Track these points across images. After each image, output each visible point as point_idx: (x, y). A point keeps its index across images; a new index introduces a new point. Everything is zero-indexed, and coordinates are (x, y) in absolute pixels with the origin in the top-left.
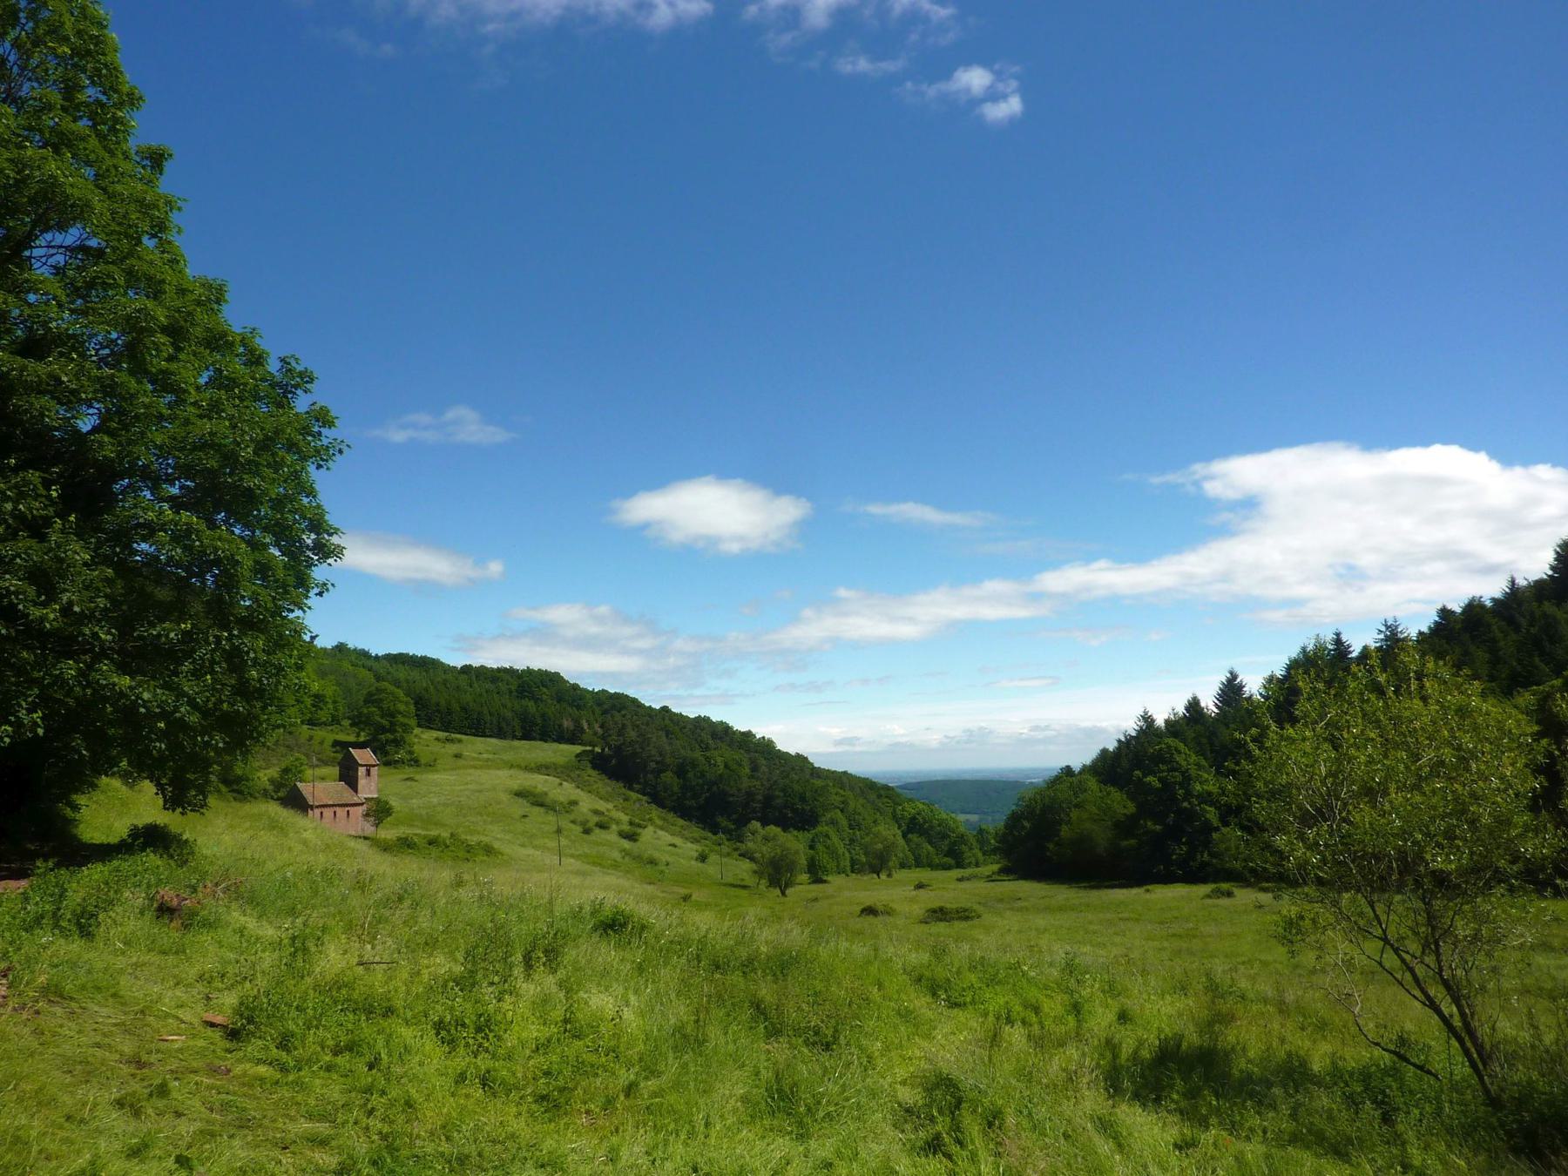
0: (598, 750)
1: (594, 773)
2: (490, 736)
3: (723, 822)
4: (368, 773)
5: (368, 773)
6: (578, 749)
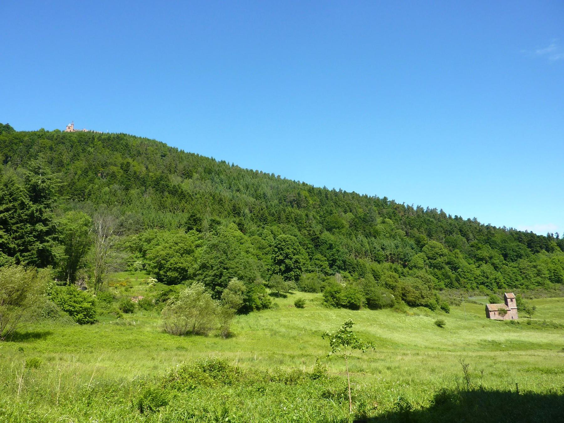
4: (512, 301)
5: (512, 301)
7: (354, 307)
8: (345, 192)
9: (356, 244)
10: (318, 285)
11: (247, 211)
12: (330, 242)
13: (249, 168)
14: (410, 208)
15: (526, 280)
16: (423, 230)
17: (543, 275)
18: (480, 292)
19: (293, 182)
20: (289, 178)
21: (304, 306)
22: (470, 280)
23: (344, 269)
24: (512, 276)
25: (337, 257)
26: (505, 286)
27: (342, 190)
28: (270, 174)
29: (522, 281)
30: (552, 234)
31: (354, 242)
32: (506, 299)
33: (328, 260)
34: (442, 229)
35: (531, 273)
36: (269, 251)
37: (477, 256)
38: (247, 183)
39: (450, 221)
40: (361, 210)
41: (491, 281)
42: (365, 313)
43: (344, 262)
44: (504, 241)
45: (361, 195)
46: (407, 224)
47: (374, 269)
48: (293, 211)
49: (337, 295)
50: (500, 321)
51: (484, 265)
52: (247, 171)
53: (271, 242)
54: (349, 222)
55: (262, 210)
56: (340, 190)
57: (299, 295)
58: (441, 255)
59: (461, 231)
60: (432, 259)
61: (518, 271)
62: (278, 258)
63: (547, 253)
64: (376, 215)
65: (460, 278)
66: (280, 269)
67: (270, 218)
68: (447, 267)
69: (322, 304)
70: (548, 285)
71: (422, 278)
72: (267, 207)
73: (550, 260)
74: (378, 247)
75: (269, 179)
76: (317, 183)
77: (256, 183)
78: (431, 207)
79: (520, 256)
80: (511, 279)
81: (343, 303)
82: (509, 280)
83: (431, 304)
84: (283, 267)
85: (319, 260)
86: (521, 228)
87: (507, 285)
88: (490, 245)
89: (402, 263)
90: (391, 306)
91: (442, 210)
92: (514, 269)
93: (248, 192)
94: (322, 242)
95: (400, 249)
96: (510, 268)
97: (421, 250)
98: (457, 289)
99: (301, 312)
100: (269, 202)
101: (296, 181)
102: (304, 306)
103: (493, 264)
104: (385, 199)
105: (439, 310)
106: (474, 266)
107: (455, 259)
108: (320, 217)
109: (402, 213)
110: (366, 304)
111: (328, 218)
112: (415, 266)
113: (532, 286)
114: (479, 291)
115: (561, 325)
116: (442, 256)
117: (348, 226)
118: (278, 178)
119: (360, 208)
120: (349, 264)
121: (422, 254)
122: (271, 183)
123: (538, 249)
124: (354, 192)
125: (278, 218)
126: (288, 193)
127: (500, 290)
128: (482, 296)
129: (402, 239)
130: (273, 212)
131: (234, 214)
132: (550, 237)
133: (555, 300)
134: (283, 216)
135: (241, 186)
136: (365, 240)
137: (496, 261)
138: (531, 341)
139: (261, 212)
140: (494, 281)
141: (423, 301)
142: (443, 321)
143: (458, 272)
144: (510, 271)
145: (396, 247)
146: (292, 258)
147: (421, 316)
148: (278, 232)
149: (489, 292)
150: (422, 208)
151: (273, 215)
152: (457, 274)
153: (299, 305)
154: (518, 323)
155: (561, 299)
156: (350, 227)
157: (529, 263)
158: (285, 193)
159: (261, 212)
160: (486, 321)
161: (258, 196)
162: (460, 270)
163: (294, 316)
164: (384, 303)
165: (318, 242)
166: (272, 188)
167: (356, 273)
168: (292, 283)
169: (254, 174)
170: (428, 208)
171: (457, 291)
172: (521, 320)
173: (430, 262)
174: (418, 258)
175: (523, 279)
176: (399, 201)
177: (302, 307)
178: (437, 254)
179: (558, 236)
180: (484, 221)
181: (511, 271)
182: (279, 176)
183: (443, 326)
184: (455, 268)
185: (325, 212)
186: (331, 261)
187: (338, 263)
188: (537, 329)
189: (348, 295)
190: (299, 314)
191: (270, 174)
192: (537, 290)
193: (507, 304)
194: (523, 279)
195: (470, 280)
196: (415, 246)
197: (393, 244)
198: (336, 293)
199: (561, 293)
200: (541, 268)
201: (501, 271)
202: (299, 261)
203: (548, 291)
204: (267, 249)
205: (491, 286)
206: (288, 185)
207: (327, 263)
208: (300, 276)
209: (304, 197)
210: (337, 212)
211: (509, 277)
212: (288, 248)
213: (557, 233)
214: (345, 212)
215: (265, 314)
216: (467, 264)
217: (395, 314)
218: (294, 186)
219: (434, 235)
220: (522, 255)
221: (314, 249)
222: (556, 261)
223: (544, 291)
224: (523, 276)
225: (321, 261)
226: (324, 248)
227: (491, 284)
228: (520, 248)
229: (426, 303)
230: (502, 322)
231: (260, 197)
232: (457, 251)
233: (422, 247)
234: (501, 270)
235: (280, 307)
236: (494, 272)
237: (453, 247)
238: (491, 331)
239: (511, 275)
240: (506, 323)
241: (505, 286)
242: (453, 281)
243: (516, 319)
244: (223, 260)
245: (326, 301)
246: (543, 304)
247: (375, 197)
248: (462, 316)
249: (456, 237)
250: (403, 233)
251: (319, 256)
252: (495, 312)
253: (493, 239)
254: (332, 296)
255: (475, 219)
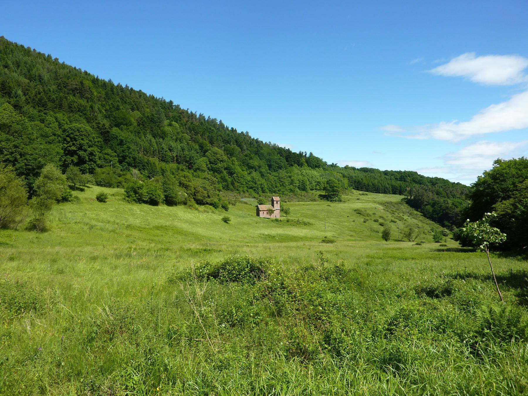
0: (409, 198)
1: (406, 205)
2: (381, 193)
3: (446, 223)
4: (277, 203)
5: (277, 203)
6: (403, 197)
7: (153, 202)
8: (132, 89)
9: (145, 143)
10: (115, 179)
11: (20, 92)
12: (121, 138)
13: (20, 43)
14: (192, 115)
16: (206, 137)
18: (249, 195)
19: (74, 69)
20: (68, 63)
21: (106, 200)
22: (242, 184)
23: (133, 167)
25: (127, 154)
26: (267, 191)
27: (128, 87)
28: (46, 55)
30: (303, 153)
31: (143, 140)
32: (273, 201)
33: (118, 156)
34: (221, 138)
35: (287, 182)
36: (54, 141)
37: (249, 164)
38: (17, 60)
39: (227, 132)
40: (148, 110)
42: (163, 208)
43: (134, 159)
44: (269, 154)
45: (148, 95)
46: (192, 129)
47: (163, 169)
48: (76, 100)
49: (140, 191)
51: (254, 173)
52: (17, 46)
53: (55, 131)
54: (137, 120)
55: (39, 94)
56: (127, 87)
57: (97, 190)
58: (222, 161)
59: (236, 142)
60: (213, 164)
62: (70, 149)
63: (298, 167)
64: (163, 116)
66: (72, 160)
67: (49, 104)
68: (225, 172)
69: (124, 199)
70: (297, 192)
71: (209, 180)
72: (44, 91)
73: (300, 173)
74: (166, 148)
75: (45, 60)
76: (103, 75)
77: (29, 62)
78: (212, 117)
79: (280, 168)
81: (144, 199)
83: (215, 203)
84: (75, 159)
85: (108, 154)
86: (281, 145)
87: (269, 190)
88: (259, 156)
89: (187, 165)
90: (185, 204)
91: (221, 121)
92: (275, 178)
93: (19, 70)
94: (112, 137)
95: (186, 152)
96: (272, 176)
97: (204, 155)
99: (105, 206)
100: (46, 86)
101: (77, 68)
102: (106, 200)
103: (261, 172)
104: (171, 102)
105: (220, 208)
106: (246, 173)
107: (232, 166)
108: (105, 111)
109: (186, 119)
110: (164, 200)
111: (116, 113)
112: (199, 169)
113: (286, 192)
115: (308, 223)
116: (222, 162)
117: (135, 124)
118: (55, 61)
119: (147, 108)
120: (139, 161)
121: (205, 158)
122: (47, 65)
123: (293, 163)
124: (140, 91)
125: (59, 105)
126: (70, 80)
127: (264, 194)
129: (188, 144)
130: (53, 98)
131: (3, 93)
132: (301, 154)
133: (302, 204)
134: (65, 104)
135: (9, 63)
136: (153, 140)
137: (263, 170)
138: (293, 234)
139: (39, 96)
140: (260, 186)
141: (209, 200)
143: (233, 177)
145: (182, 150)
146: (87, 150)
147: (210, 213)
148: (64, 120)
149: (256, 195)
150: (204, 117)
151: (53, 101)
153: (101, 199)
155: (306, 203)
156: (139, 125)
157: (286, 174)
158: (65, 80)
159: (39, 96)
160: (257, 219)
161: (32, 77)
162: (235, 175)
163: (99, 210)
164: (180, 201)
165: (108, 137)
166: (49, 71)
167: (146, 171)
168: (88, 176)
169: (27, 52)
170: (209, 117)
172: (282, 218)
173: (211, 167)
174: (202, 162)
176: (183, 107)
177: (104, 202)
178: (218, 159)
179: (306, 155)
180: (254, 135)
182: (56, 59)
183: (228, 222)
184: (231, 174)
185: (111, 106)
186: (121, 157)
187: (128, 160)
189: (150, 191)
190: (104, 208)
191: (46, 55)
193: (273, 205)
195: (242, 184)
196: (199, 151)
197: (179, 147)
198: (138, 189)
199: (305, 199)
202: (94, 154)
204: (51, 138)
206: (68, 71)
207: (117, 159)
208: (95, 169)
209: (88, 88)
210: (124, 109)
212: (82, 139)
213: (306, 152)
214: (133, 110)
215: (67, 207)
216: (241, 171)
217: (189, 210)
218: (74, 73)
219: (215, 143)
220: (282, 167)
221: (103, 143)
222: (304, 174)
224: (281, 184)
225: (111, 156)
226: (115, 143)
227: (258, 188)
228: (281, 161)
229: (211, 202)
231: (34, 78)
232: (234, 158)
233: (205, 152)
235: (82, 200)
236: (261, 179)
237: (230, 155)
239: (272, 182)
240: (272, 221)
241: (267, 191)
243: (278, 217)
244: (18, 143)
245: (127, 197)
247: (162, 99)
249: (233, 146)
250: (188, 137)
251: (109, 151)
253: (262, 151)
254: (136, 192)
255: (247, 133)
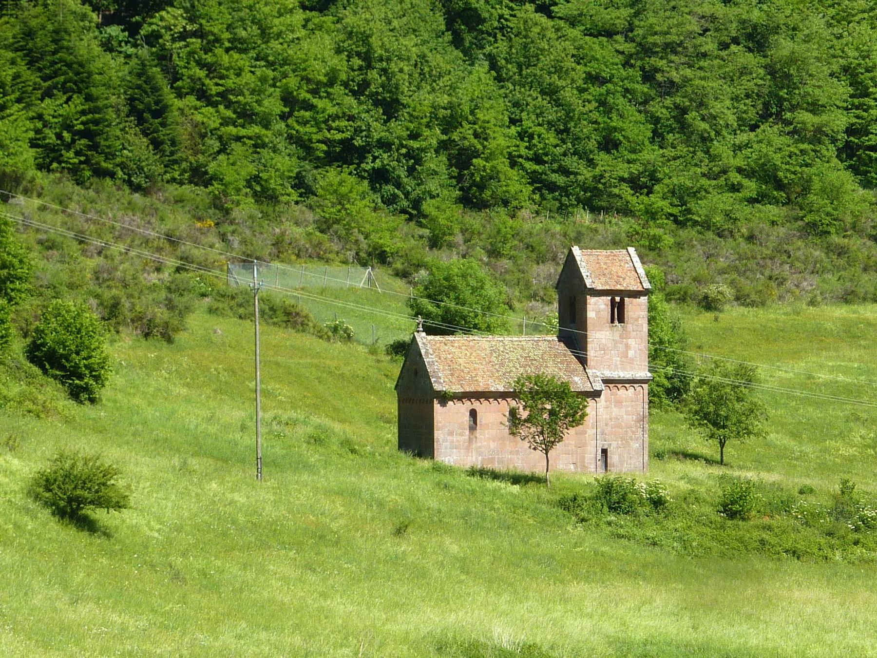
4: (618, 313)
5: (618, 313)
15: (682, 149)
17: (806, 117)
18: (324, 226)
22: (246, 116)
24: (579, 108)
29: (651, 154)
41: (414, 136)
50: (516, 479)
61: (626, 64)
65: (170, 98)
80: (563, 132)
82: (551, 138)
87: (534, 179)
92: (602, 49)
98: (136, 188)
114: (310, 216)
127: (475, 220)
128: (336, 268)
142: (107, 473)
143: (153, 39)
144: (569, 63)
152: (144, 52)
154: (658, 503)
171: (131, 206)
175: (657, 136)
181: (579, 59)
183: (99, 515)
188: (795, 553)
192: (751, 238)
194: (657, 136)
195: (246, 116)
200: (799, 48)
201: (492, 60)
203: (829, 249)
205: (409, 183)
211: (552, 114)
223: (800, 248)
224: (661, 108)
227: (415, 158)
230: (532, 490)
234: (501, 47)
238: (464, 565)
239: (569, 95)
242: (111, 114)
246: (796, 355)
248: (213, 429)
252: (483, 408)
